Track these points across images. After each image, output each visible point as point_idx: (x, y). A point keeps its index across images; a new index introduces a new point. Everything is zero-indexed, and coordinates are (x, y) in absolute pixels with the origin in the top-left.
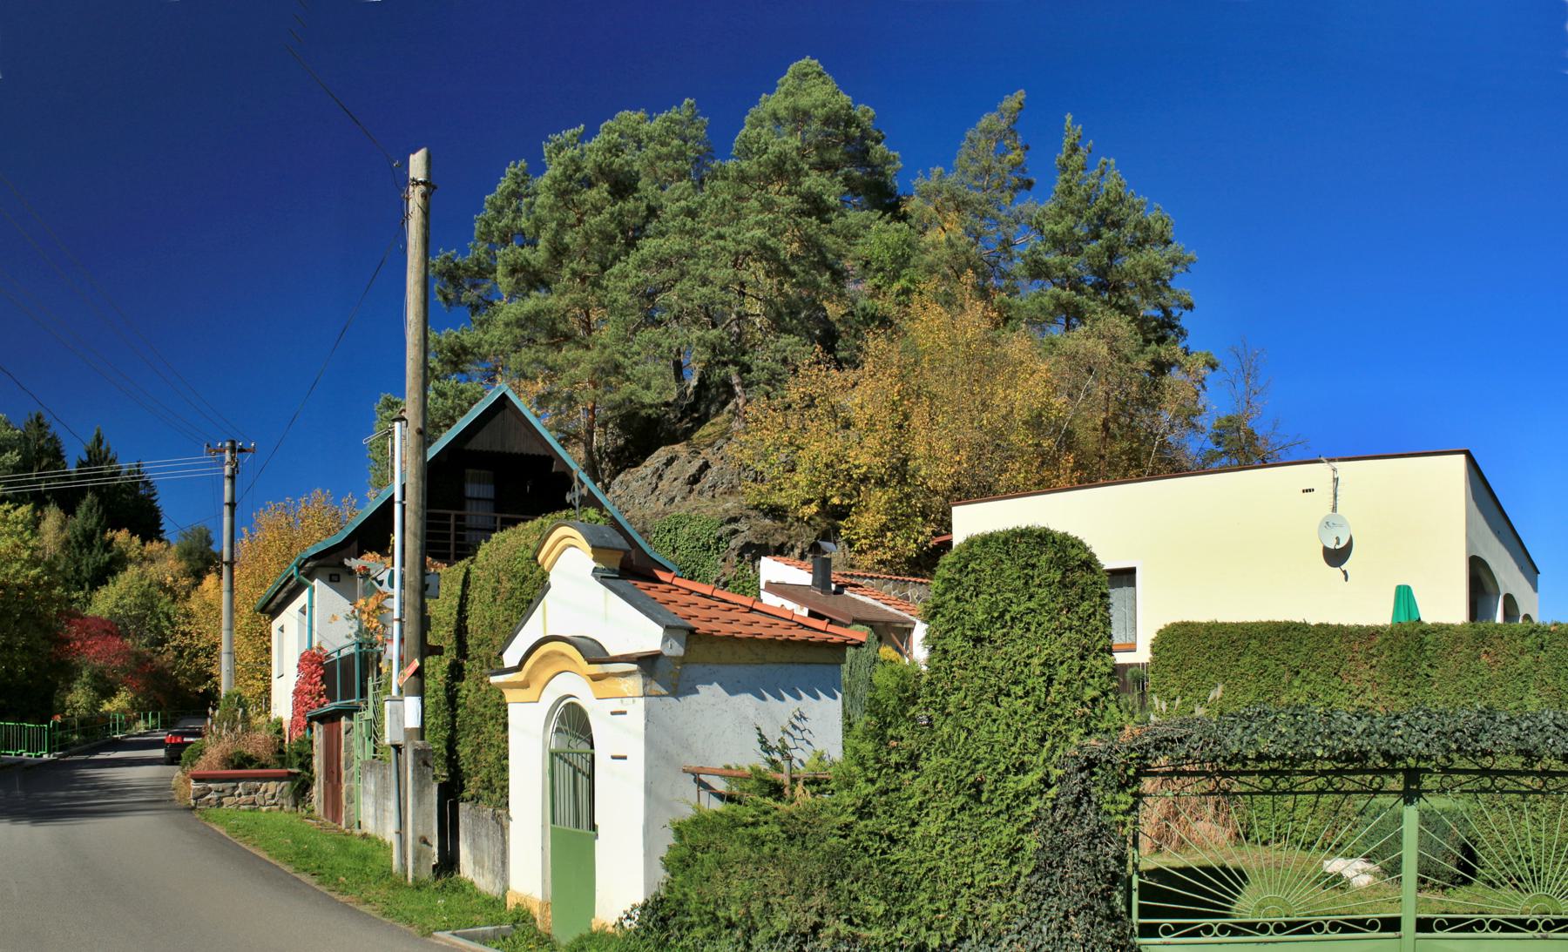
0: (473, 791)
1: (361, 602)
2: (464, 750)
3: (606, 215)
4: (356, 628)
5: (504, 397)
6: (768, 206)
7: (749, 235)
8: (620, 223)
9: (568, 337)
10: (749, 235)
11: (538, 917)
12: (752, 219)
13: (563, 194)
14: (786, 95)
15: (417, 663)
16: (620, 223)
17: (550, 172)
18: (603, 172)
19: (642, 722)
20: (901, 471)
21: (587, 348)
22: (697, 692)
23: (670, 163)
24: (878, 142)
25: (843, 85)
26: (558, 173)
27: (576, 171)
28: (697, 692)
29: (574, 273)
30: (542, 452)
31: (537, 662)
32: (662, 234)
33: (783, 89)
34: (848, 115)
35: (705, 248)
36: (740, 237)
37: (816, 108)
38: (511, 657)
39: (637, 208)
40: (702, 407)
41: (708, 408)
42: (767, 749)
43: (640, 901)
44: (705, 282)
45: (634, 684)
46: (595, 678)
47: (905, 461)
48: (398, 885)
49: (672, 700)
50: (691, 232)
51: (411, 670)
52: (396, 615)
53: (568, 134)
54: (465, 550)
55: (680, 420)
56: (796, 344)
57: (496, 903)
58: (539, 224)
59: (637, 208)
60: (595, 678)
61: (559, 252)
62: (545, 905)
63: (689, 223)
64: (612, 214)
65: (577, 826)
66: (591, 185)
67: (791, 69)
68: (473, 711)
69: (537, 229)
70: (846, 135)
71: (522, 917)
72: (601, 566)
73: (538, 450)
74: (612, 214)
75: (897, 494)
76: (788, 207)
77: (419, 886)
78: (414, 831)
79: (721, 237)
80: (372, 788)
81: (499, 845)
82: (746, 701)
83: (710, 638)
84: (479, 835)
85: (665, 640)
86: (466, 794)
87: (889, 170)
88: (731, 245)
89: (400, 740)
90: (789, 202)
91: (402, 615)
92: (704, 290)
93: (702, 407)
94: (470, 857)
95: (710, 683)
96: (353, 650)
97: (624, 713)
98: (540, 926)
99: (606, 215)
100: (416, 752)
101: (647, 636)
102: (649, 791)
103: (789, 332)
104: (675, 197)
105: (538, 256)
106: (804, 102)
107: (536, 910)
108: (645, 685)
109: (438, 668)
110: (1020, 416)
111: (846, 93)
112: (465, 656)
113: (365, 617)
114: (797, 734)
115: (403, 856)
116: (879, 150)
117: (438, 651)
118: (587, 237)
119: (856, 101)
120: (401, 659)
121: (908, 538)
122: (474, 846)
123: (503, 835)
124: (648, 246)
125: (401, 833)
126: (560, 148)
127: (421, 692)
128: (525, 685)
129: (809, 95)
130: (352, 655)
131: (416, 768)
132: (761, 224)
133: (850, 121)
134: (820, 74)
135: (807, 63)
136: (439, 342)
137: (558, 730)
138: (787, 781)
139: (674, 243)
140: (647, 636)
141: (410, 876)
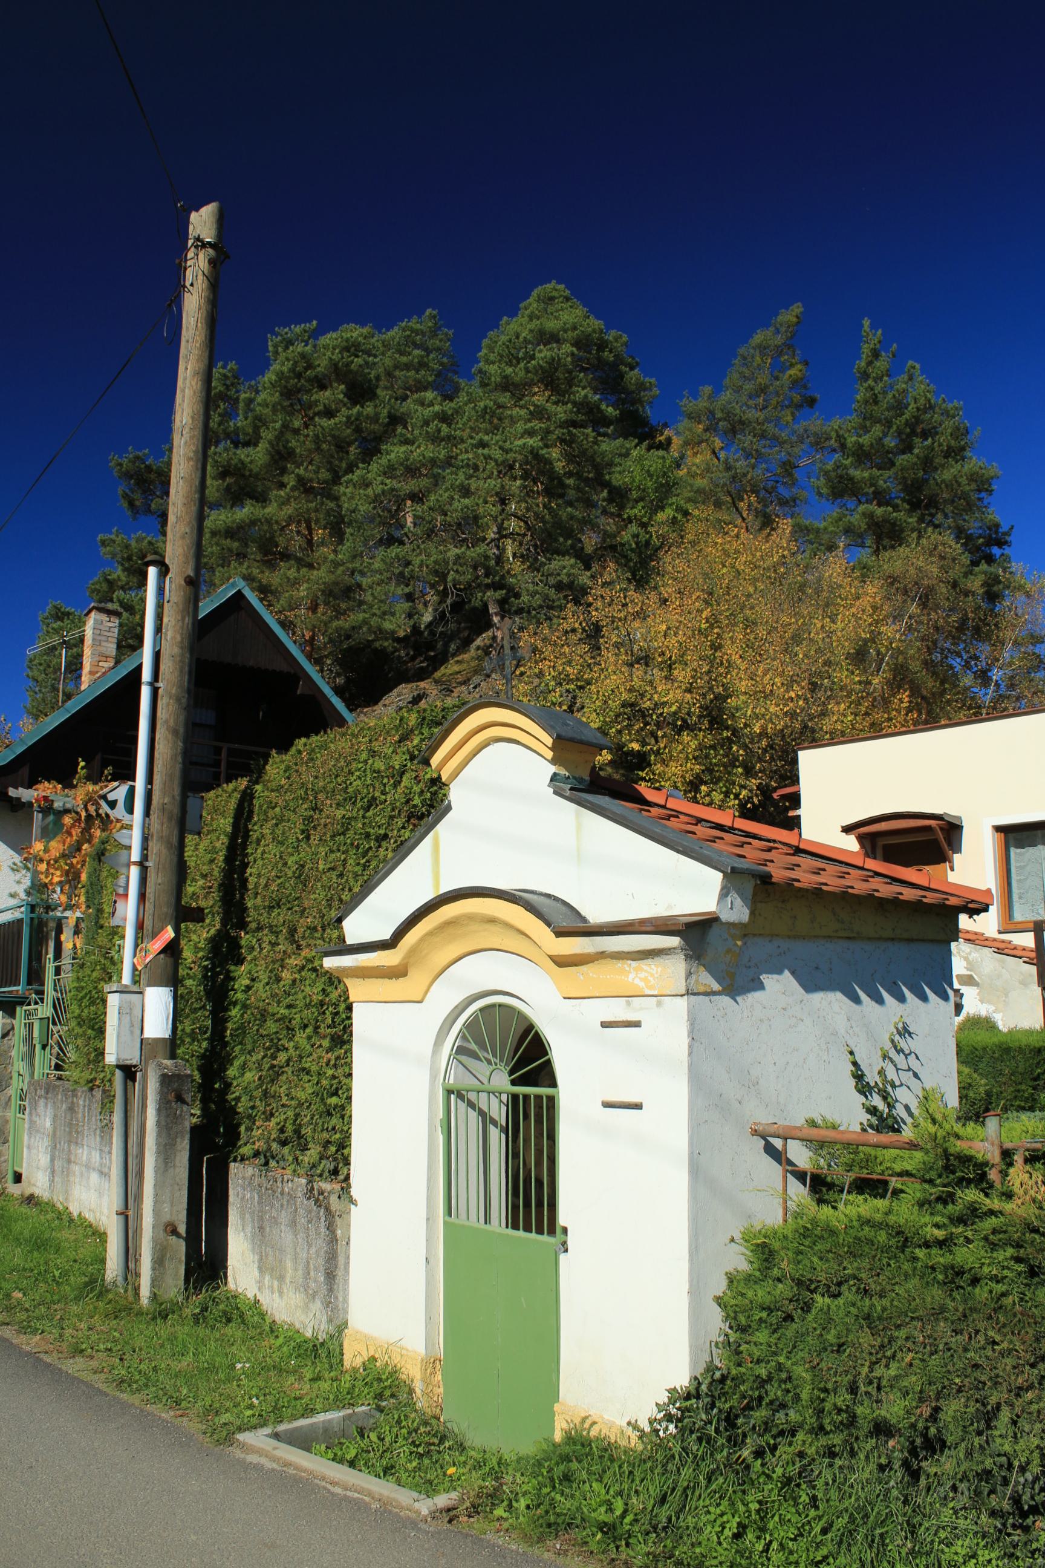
0: (260, 1145)
1: (38, 847)
2: (243, 1076)
3: (340, 418)
4: (27, 882)
5: (239, 594)
6: (539, 413)
7: (520, 442)
8: (358, 430)
9: (285, 556)
10: (520, 442)
11: (418, 1387)
12: (520, 427)
13: (291, 394)
14: (531, 318)
15: (170, 933)
16: (358, 430)
17: (276, 367)
18: (339, 372)
19: (685, 1041)
20: (715, 714)
21: (311, 566)
22: (761, 987)
23: (412, 373)
24: (632, 369)
25: (594, 310)
26: (285, 369)
27: (306, 369)
28: (761, 987)
29: (301, 481)
30: (284, 667)
31: (431, 934)
32: (407, 442)
33: (528, 312)
34: (600, 339)
35: (464, 456)
36: (507, 445)
37: (565, 331)
38: (364, 923)
39: (377, 414)
40: (440, 645)
41: (446, 646)
42: (864, 1088)
43: (682, 1380)
44: (466, 492)
45: (672, 971)
46: (562, 962)
47: (721, 699)
48: (124, 1308)
49: (726, 1000)
50: (449, 438)
51: (158, 945)
52: (135, 856)
53: (298, 329)
54: (250, 766)
55: (413, 659)
56: (572, 566)
57: (322, 1352)
58: (260, 422)
59: (377, 414)
60: (562, 962)
61: (281, 457)
62: (431, 1363)
63: (444, 428)
64: (348, 417)
65: (487, 1220)
66: (323, 387)
67: (535, 293)
68: (264, 1015)
69: (256, 429)
70: (599, 359)
71: (383, 1386)
72: (563, 772)
73: (282, 666)
74: (348, 417)
75: (709, 740)
76: (562, 416)
77: (162, 1312)
78: (156, 1212)
79: (483, 445)
80: (46, 1122)
81: (320, 1244)
82: (833, 1002)
83: (789, 891)
84: (275, 1221)
85: (724, 894)
86: (246, 1150)
87: (645, 395)
88: (497, 454)
89: (133, 1057)
90: (561, 412)
91: (145, 857)
92: (466, 501)
93: (440, 645)
94: (252, 1258)
95: (780, 972)
96: (18, 915)
97: (637, 1024)
98: (422, 1403)
99: (340, 418)
100: (166, 1080)
101: (694, 888)
102: (696, 1170)
103: (563, 554)
104: (426, 406)
105: (257, 456)
106: (551, 325)
107: (413, 1372)
108: (689, 974)
109: (199, 937)
110: (843, 648)
111: (598, 318)
112: (242, 925)
113: (43, 867)
114: (900, 1059)
115: (130, 1253)
116: (633, 376)
117: (197, 915)
118: (317, 440)
119: (609, 327)
120: (140, 926)
121: (727, 794)
122: (261, 1234)
123: (331, 1227)
124: (395, 452)
125: (128, 1214)
126: (289, 343)
127: (174, 981)
128: (398, 973)
129: (557, 318)
130: (20, 921)
131: (164, 1107)
132: (530, 433)
133: (602, 345)
134: (567, 299)
135: (550, 287)
136: (127, 547)
137: (461, 1051)
138: (995, 1157)
139: (424, 450)
140: (694, 888)
141: (145, 1292)
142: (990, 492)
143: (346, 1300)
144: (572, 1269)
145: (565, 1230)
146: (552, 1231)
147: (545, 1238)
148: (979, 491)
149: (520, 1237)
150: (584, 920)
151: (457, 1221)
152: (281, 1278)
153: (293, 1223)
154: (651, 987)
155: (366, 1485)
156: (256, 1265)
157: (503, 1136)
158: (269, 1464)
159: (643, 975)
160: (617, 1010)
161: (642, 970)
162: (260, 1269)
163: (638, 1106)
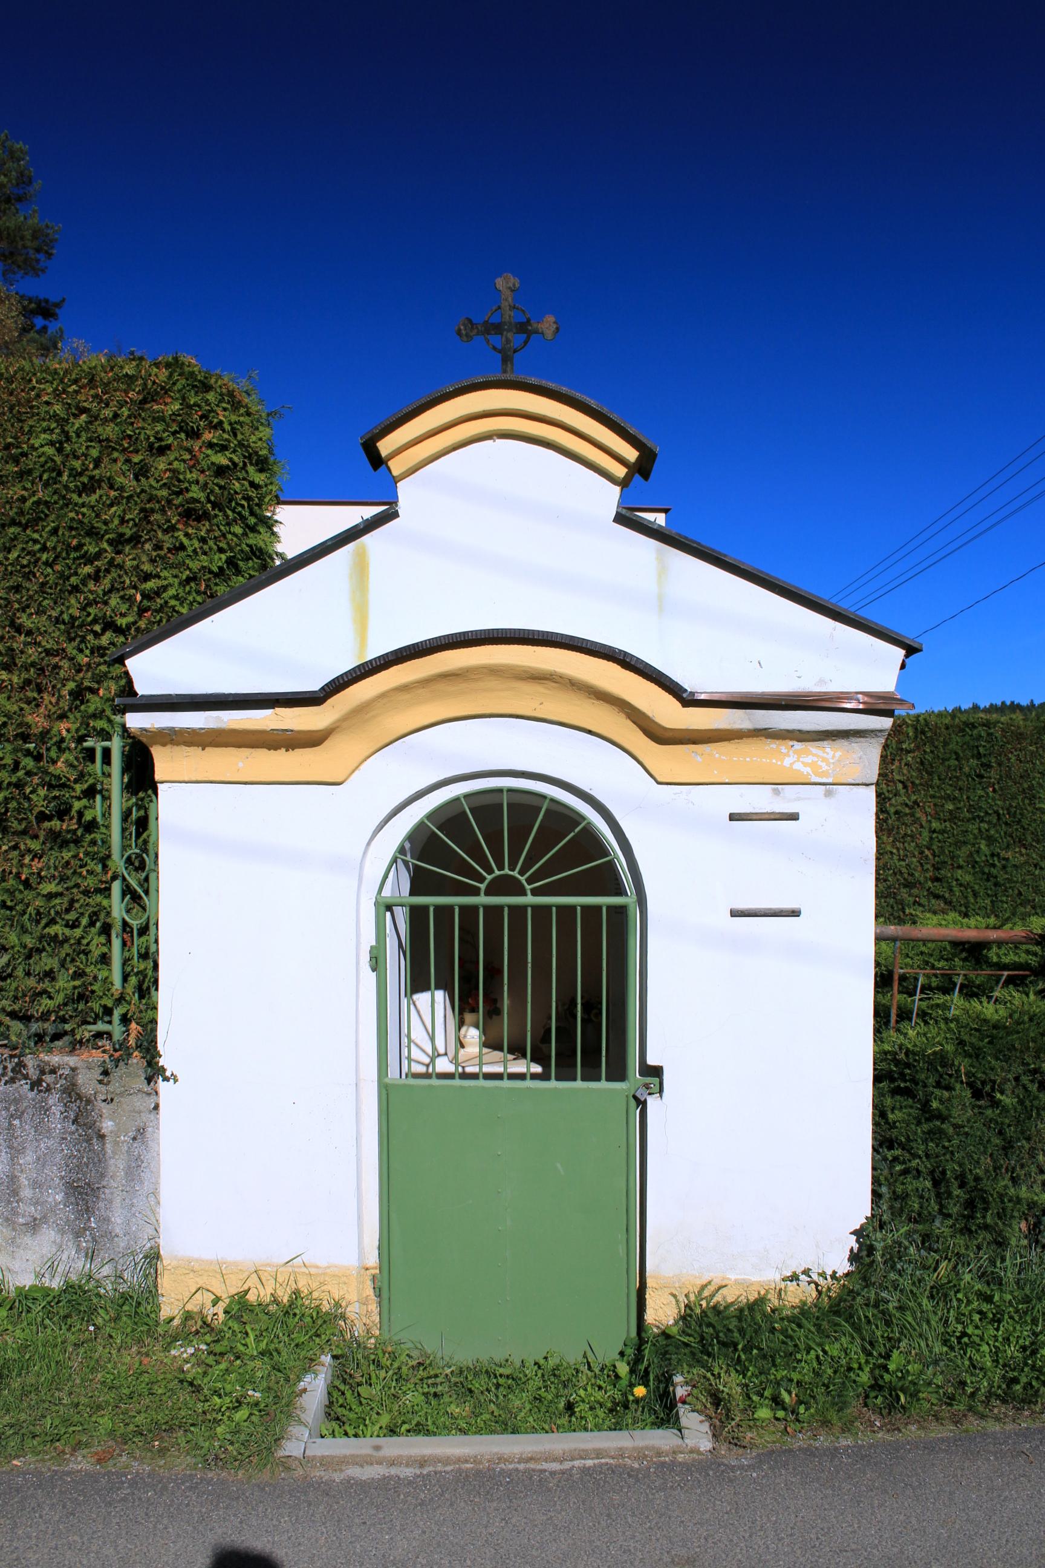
31: (405, 688)
97: (794, 817)
142: (49, 255)
148: (38, 250)
154: (825, 774)
155: (589, 1446)
157: (370, 978)
158: (408, 1472)
159: (809, 759)
160: (759, 799)
161: (808, 753)
163: (795, 913)
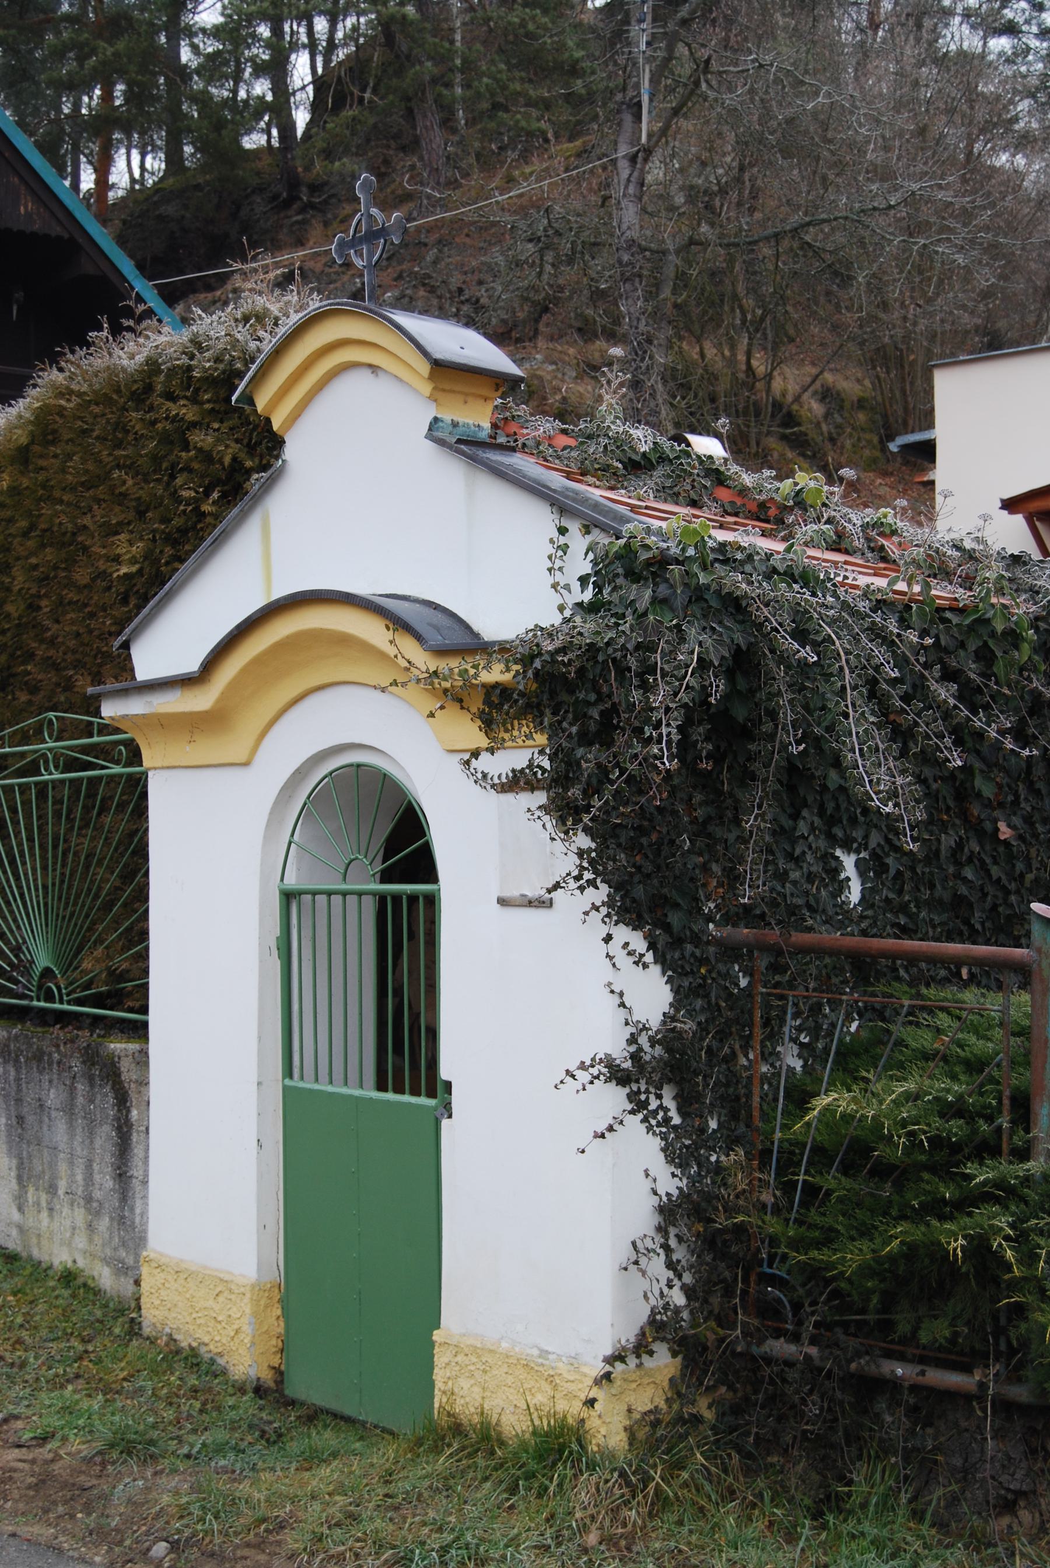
38: (169, 643)
123: (122, 1100)
143: (144, 1214)
144: (453, 1134)
145: (448, 1085)
146: (432, 1094)
147: (423, 1100)
149: (388, 1102)
150: (477, 636)
151: (301, 1085)
152: (52, 1189)
153: (69, 1108)
156: (13, 1174)
162: (19, 1178)
